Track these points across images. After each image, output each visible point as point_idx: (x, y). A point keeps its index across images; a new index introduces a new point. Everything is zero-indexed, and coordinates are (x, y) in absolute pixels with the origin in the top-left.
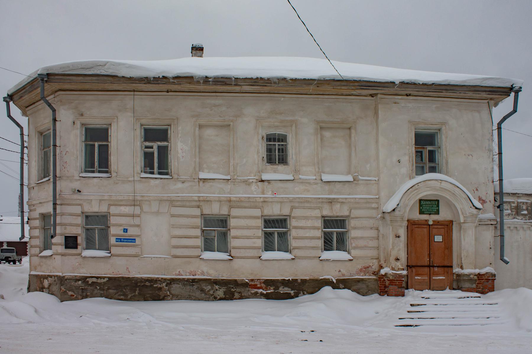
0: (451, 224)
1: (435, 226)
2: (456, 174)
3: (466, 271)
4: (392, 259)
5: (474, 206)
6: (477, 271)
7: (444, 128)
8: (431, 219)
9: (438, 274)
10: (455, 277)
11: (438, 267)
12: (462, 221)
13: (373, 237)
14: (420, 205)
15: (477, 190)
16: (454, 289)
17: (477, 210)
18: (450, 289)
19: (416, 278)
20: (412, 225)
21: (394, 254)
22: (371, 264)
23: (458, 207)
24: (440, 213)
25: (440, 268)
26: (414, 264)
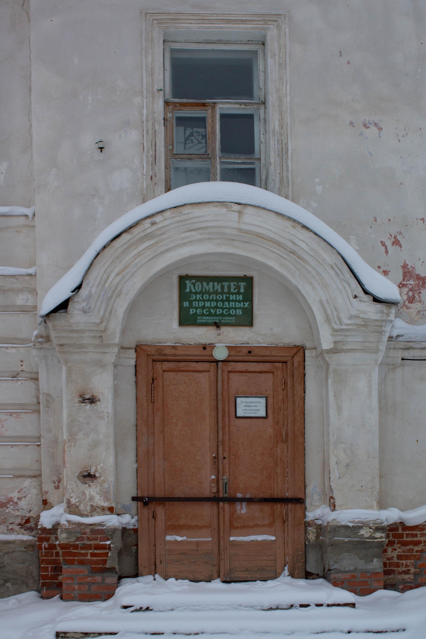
0: (297, 359)
1: (240, 367)
2: (319, 189)
3: (346, 516)
4: (70, 474)
5: (366, 292)
6: (391, 515)
7: (272, 34)
8: (223, 340)
9: (248, 527)
10: (312, 537)
11: (250, 501)
12: (326, 345)
13: (22, 406)
14: (183, 296)
15: (396, 242)
16: (308, 575)
17: (378, 306)
18: (292, 575)
19: (169, 538)
20: (153, 365)
21: (76, 458)
22: (15, 495)
23: (312, 295)
24: (256, 321)
25: (255, 507)
26: (159, 494)
